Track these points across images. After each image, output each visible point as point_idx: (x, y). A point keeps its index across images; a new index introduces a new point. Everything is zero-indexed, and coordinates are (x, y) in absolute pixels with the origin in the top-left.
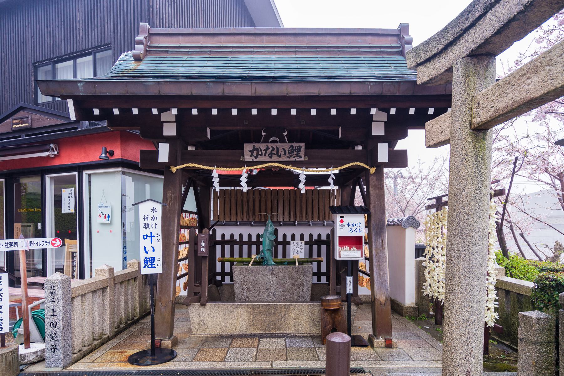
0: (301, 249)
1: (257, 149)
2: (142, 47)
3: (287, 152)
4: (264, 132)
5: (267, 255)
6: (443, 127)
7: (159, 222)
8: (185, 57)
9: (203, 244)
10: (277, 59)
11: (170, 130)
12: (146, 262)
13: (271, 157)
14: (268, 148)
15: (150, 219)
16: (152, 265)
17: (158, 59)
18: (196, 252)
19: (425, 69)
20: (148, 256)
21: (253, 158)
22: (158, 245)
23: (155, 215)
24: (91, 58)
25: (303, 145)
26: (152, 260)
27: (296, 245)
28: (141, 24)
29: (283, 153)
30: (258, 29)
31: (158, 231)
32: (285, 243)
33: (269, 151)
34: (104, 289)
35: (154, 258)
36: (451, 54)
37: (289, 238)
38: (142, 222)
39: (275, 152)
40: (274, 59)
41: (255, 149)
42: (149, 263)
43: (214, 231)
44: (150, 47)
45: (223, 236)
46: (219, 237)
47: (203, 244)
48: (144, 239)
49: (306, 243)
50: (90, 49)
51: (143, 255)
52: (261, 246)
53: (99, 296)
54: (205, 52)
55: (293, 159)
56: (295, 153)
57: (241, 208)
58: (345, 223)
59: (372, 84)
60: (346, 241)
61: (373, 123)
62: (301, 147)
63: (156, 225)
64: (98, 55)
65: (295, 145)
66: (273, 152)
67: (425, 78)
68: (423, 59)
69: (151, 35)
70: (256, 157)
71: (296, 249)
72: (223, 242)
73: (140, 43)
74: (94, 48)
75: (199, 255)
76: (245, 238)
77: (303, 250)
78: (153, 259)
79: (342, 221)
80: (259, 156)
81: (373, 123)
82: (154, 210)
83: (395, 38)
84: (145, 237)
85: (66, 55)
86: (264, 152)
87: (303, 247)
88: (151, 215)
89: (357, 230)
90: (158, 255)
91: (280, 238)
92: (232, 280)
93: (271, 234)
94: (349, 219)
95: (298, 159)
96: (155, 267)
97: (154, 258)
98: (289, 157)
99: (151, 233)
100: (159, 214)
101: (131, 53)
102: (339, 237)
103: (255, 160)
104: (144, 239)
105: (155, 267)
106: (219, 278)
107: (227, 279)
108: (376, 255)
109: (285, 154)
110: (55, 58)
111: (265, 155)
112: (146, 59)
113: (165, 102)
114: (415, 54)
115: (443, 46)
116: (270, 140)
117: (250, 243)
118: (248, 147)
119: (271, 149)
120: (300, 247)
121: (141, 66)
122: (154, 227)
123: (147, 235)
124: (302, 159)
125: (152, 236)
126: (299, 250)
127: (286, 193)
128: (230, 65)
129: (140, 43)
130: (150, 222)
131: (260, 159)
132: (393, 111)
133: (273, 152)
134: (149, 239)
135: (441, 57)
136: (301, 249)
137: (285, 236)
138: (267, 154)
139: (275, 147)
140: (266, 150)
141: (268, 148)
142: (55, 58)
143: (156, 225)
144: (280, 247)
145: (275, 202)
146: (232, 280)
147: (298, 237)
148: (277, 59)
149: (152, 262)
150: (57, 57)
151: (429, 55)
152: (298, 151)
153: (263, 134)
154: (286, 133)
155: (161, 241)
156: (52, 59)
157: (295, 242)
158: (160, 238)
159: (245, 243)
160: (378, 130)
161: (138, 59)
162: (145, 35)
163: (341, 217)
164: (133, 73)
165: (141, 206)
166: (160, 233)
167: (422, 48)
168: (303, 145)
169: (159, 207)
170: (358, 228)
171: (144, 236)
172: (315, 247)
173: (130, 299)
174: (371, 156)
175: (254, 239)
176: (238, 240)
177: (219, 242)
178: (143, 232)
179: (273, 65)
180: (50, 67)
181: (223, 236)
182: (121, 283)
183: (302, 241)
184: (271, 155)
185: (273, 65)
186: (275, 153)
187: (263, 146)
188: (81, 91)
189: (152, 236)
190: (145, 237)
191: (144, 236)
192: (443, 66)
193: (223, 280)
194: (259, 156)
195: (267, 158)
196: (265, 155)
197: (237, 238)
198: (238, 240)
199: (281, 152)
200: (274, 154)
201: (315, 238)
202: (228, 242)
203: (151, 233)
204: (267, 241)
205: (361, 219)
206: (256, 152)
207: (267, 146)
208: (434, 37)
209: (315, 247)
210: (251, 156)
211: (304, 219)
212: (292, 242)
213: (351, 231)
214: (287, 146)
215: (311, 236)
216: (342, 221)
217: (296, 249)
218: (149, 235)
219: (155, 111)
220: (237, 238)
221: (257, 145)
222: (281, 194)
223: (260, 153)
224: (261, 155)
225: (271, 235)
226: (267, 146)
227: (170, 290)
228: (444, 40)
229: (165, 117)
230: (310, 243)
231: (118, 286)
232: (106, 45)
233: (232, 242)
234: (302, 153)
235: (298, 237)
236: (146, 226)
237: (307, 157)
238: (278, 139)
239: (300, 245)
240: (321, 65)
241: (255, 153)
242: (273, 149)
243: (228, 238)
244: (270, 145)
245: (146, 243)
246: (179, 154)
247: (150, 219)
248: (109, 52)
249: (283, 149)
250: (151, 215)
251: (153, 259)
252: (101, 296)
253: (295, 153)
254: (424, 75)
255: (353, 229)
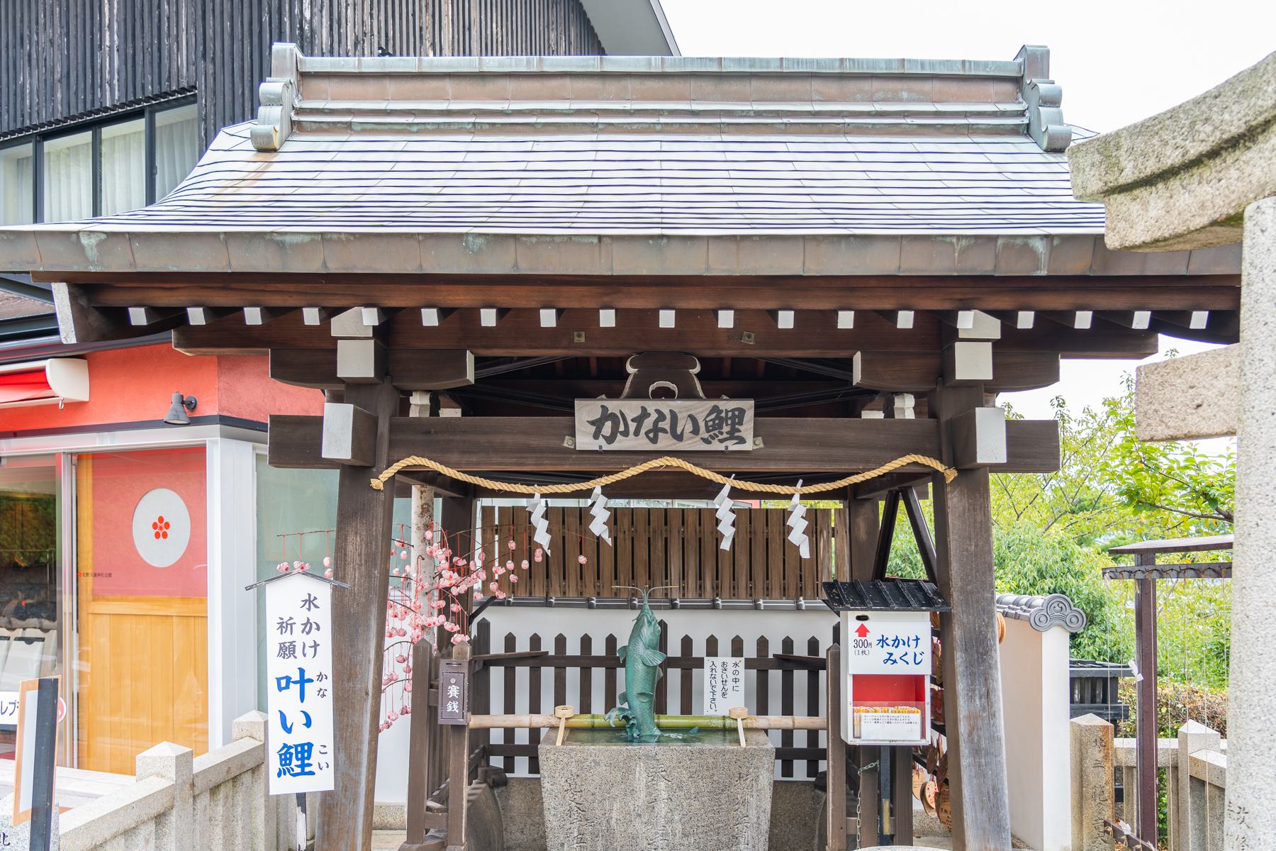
0: (736, 680)
1: (613, 417)
2: (276, 111)
3: (702, 425)
4: (632, 365)
5: (640, 707)
6: (1203, 391)
7: (325, 636)
8: (398, 142)
9: (454, 691)
10: (666, 147)
11: (356, 361)
12: (285, 757)
13: (654, 440)
14: (645, 414)
15: (298, 628)
16: (303, 766)
17: (323, 147)
18: (433, 711)
19: (1135, 208)
20: (293, 739)
21: (601, 441)
22: (322, 708)
23: (314, 615)
24: (140, 125)
25: (748, 405)
26: (303, 751)
27: (719, 669)
28: (277, 46)
29: (689, 427)
30: (615, 62)
31: (321, 663)
32: (688, 663)
33: (648, 424)
34: (160, 818)
35: (310, 745)
36: (1233, 173)
37: (699, 650)
38: (274, 639)
39: (666, 425)
40: (656, 146)
41: (606, 415)
42: (295, 762)
43: (484, 627)
44: (300, 111)
45: (510, 641)
46: (497, 647)
47: (454, 691)
48: (280, 689)
49: (749, 664)
50: (138, 102)
51: (278, 739)
52: (620, 672)
53: (147, 841)
54: (460, 129)
55: (721, 447)
56: (726, 429)
57: (564, 571)
58: (872, 637)
59: (964, 242)
60: (874, 689)
61: (957, 344)
62: (742, 411)
63: (316, 645)
64: (161, 118)
65: (727, 405)
66: (661, 425)
67: (1138, 235)
68: (1128, 176)
69: (304, 76)
70: (610, 440)
71: (719, 679)
72: (510, 662)
73: (276, 101)
74: (148, 99)
75: (440, 721)
76: (573, 649)
77: (741, 684)
78: (305, 750)
79: (862, 631)
80: (619, 437)
81: (957, 344)
82: (310, 602)
83: (1008, 88)
84: (283, 683)
85: (73, 118)
86: (632, 426)
87: (742, 676)
88: (300, 616)
89: (910, 658)
90: (322, 735)
91: (674, 650)
92: (534, 767)
93: (649, 647)
94: (884, 623)
95: (733, 446)
96: (312, 773)
97: (310, 745)
98: (707, 441)
99: (302, 671)
100: (323, 615)
101: (244, 128)
102: (855, 677)
103: (606, 447)
104: (280, 689)
105: (312, 773)
106: (497, 762)
107: (521, 765)
108: (970, 734)
109: (696, 431)
110: (42, 125)
111: (637, 433)
112: (288, 146)
113: (341, 288)
114: (1097, 158)
115: (1204, 148)
116: (651, 388)
117: (586, 662)
118: (586, 410)
119: (654, 416)
120: (731, 677)
121: (275, 167)
122: (310, 652)
123: (288, 679)
124: (748, 446)
125: (303, 681)
126: (730, 684)
127: (691, 520)
128: (531, 166)
129: (276, 101)
130: (298, 637)
131: (621, 444)
132: (1026, 320)
133: (661, 425)
134: (295, 688)
135: (1196, 178)
136: (736, 680)
137: (687, 642)
138: (643, 431)
139: (666, 412)
140: (639, 420)
141: (645, 414)
142: (42, 125)
143: (316, 645)
144: (674, 675)
145: (660, 545)
146: (534, 767)
147: (725, 646)
148: (666, 147)
149: (303, 759)
150: (50, 123)
151: (1151, 167)
152: (733, 424)
153: (630, 370)
154: (697, 369)
155: (330, 694)
156: (35, 127)
157: (718, 661)
158: (328, 684)
159: (573, 661)
160: (973, 362)
161: (266, 148)
162: (287, 79)
163: (859, 618)
164: (248, 194)
165: (272, 591)
166: (328, 670)
167: (1125, 144)
168: (748, 405)
169: (323, 593)
170: (911, 651)
171: (279, 680)
172: (775, 676)
173: (239, 830)
174: (955, 442)
175: (599, 649)
176: (552, 653)
177: (497, 661)
178: (278, 667)
179: (656, 165)
180: (27, 149)
181: (510, 641)
182: (214, 790)
183: (737, 659)
184: (655, 432)
185: (656, 165)
186: (667, 427)
187: (630, 408)
188: (96, 262)
189: (303, 681)
190: (284, 683)
191: (279, 680)
192: (1203, 206)
193: (509, 767)
194: (619, 437)
195: (641, 443)
196: (637, 433)
197: (548, 647)
198: (552, 653)
199: (685, 426)
200: (664, 431)
201: (775, 649)
202: (522, 659)
203: (302, 671)
204: (640, 667)
205: (917, 625)
206: (608, 424)
207: (644, 409)
208: (1173, 114)
209: (775, 676)
210: (596, 436)
211: (742, 591)
212: (708, 661)
213: (890, 659)
214: (701, 408)
215: (763, 643)
216: (862, 631)
217: (719, 679)
218: (296, 677)
219: (311, 317)
220: (548, 647)
221: (614, 406)
222: (675, 522)
223: (622, 428)
224: (626, 433)
225: (649, 652)
226: (644, 409)
227: (355, 828)
228: (1208, 128)
229: (339, 325)
230: (760, 665)
231: (204, 800)
232: (183, 90)
233: (536, 659)
234: (747, 429)
235: (725, 646)
236: (287, 650)
237: (759, 440)
238: (673, 387)
239: (730, 668)
240: (798, 166)
241: (607, 428)
242: (661, 417)
243: (523, 647)
244: (652, 406)
245: (285, 701)
246: (384, 427)
247: (298, 628)
248: (189, 111)
249: (690, 416)
250: (300, 616)
251: (305, 750)
252: (153, 842)
253: (726, 429)
254: (1136, 225)
255: (897, 654)
